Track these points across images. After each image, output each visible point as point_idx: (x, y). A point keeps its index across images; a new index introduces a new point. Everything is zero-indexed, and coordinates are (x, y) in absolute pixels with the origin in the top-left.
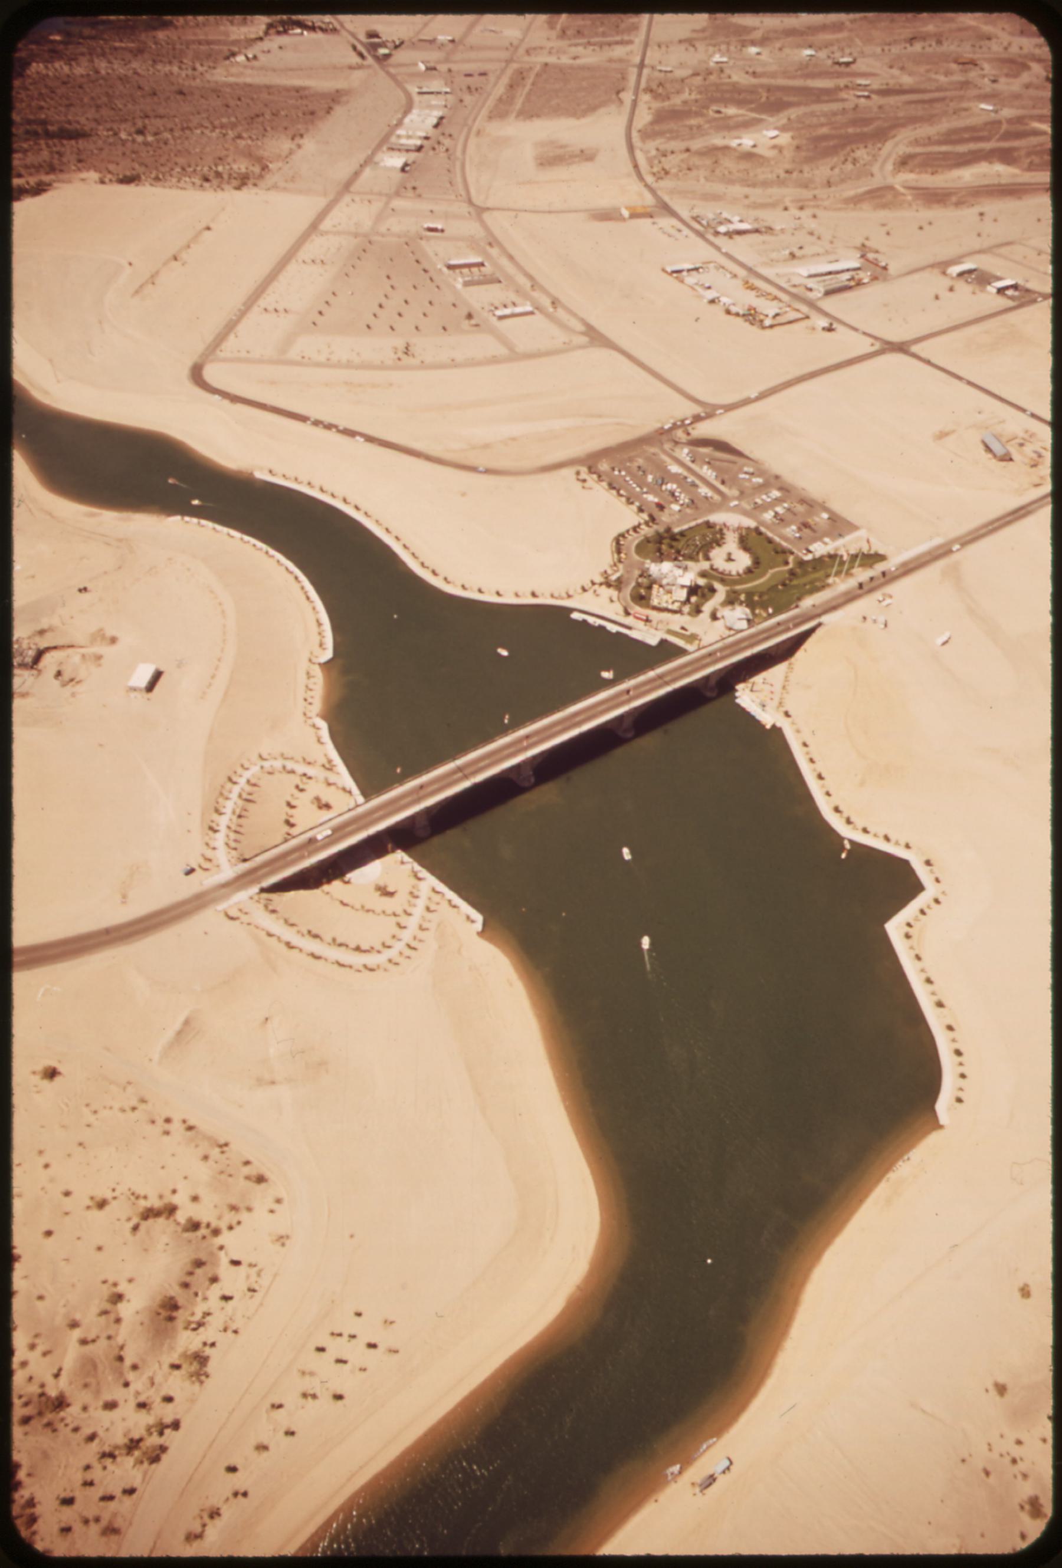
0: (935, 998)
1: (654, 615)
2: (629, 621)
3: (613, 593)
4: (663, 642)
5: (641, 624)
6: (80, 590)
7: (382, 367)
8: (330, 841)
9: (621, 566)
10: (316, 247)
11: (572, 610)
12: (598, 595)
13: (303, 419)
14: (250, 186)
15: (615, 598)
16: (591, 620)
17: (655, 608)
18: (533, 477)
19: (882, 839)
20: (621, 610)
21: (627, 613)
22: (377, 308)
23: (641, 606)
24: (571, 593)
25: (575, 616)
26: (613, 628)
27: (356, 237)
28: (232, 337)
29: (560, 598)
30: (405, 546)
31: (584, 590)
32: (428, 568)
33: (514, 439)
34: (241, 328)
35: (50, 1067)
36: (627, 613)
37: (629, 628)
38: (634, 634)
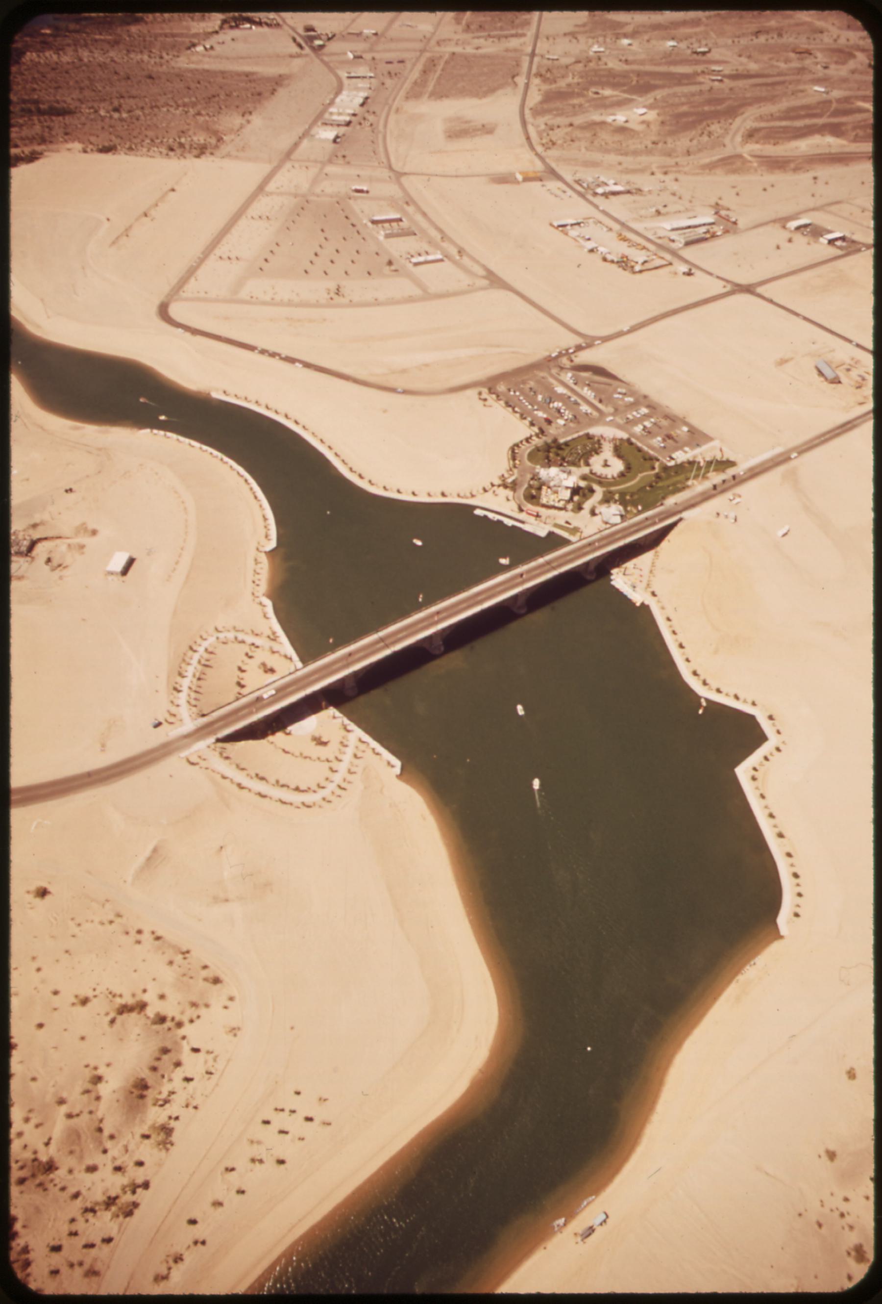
0: (777, 830)
1: (543, 511)
2: (522, 516)
3: (509, 493)
4: (551, 534)
5: (532, 519)
6: (67, 491)
7: (317, 305)
8: (274, 699)
9: (515, 471)
10: (262, 205)
11: (475, 507)
12: (496, 495)
13: (252, 348)
14: (208, 155)
15: (511, 498)
16: (491, 515)
17: (544, 506)
18: (442, 397)
20: (516, 508)
21: (521, 510)
22: (313, 256)
23: (532, 504)
24: (474, 493)
25: (478, 512)
26: (509, 522)
27: (295, 197)
28: (192, 280)
29: (465, 497)
30: (336, 454)
31: (485, 490)
32: (355, 472)
33: (427, 365)
35: (41, 887)
36: (521, 510)
37: (523, 522)
38: (526, 527)
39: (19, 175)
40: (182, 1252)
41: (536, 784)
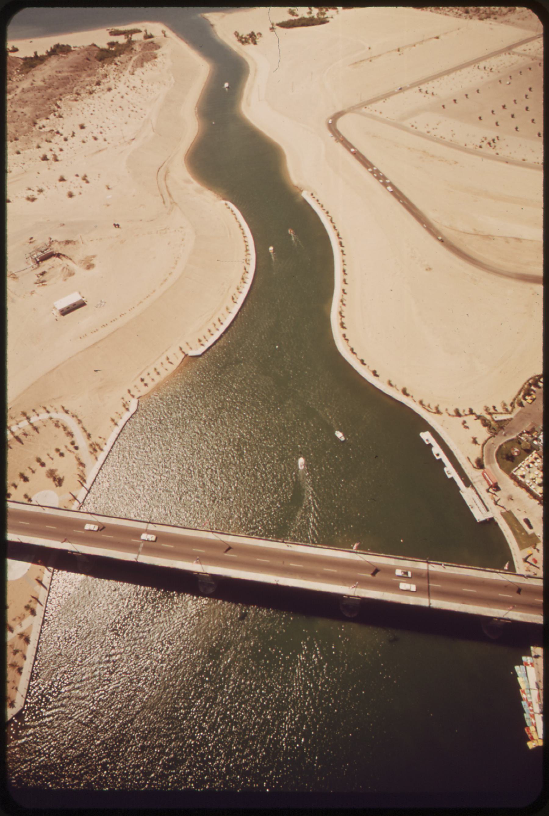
0: (325, 211)
1: (507, 484)
2: (473, 474)
3: (483, 433)
4: (491, 522)
5: (482, 487)
7: (464, 149)
9: (518, 409)
10: (493, 62)
12: (467, 427)
14: (492, 19)
15: (480, 441)
16: (437, 450)
17: (514, 478)
19: (418, 403)
20: (476, 452)
21: (480, 465)
23: (501, 467)
24: (441, 409)
25: (426, 436)
26: (450, 471)
27: (533, 60)
28: (381, 101)
29: (427, 408)
30: (341, 244)
31: (458, 414)
32: (336, 230)
33: (518, 240)
34: (390, 100)
36: (480, 465)
37: (468, 483)
38: (467, 494)
40: (58, 311)
41: (271, 248)
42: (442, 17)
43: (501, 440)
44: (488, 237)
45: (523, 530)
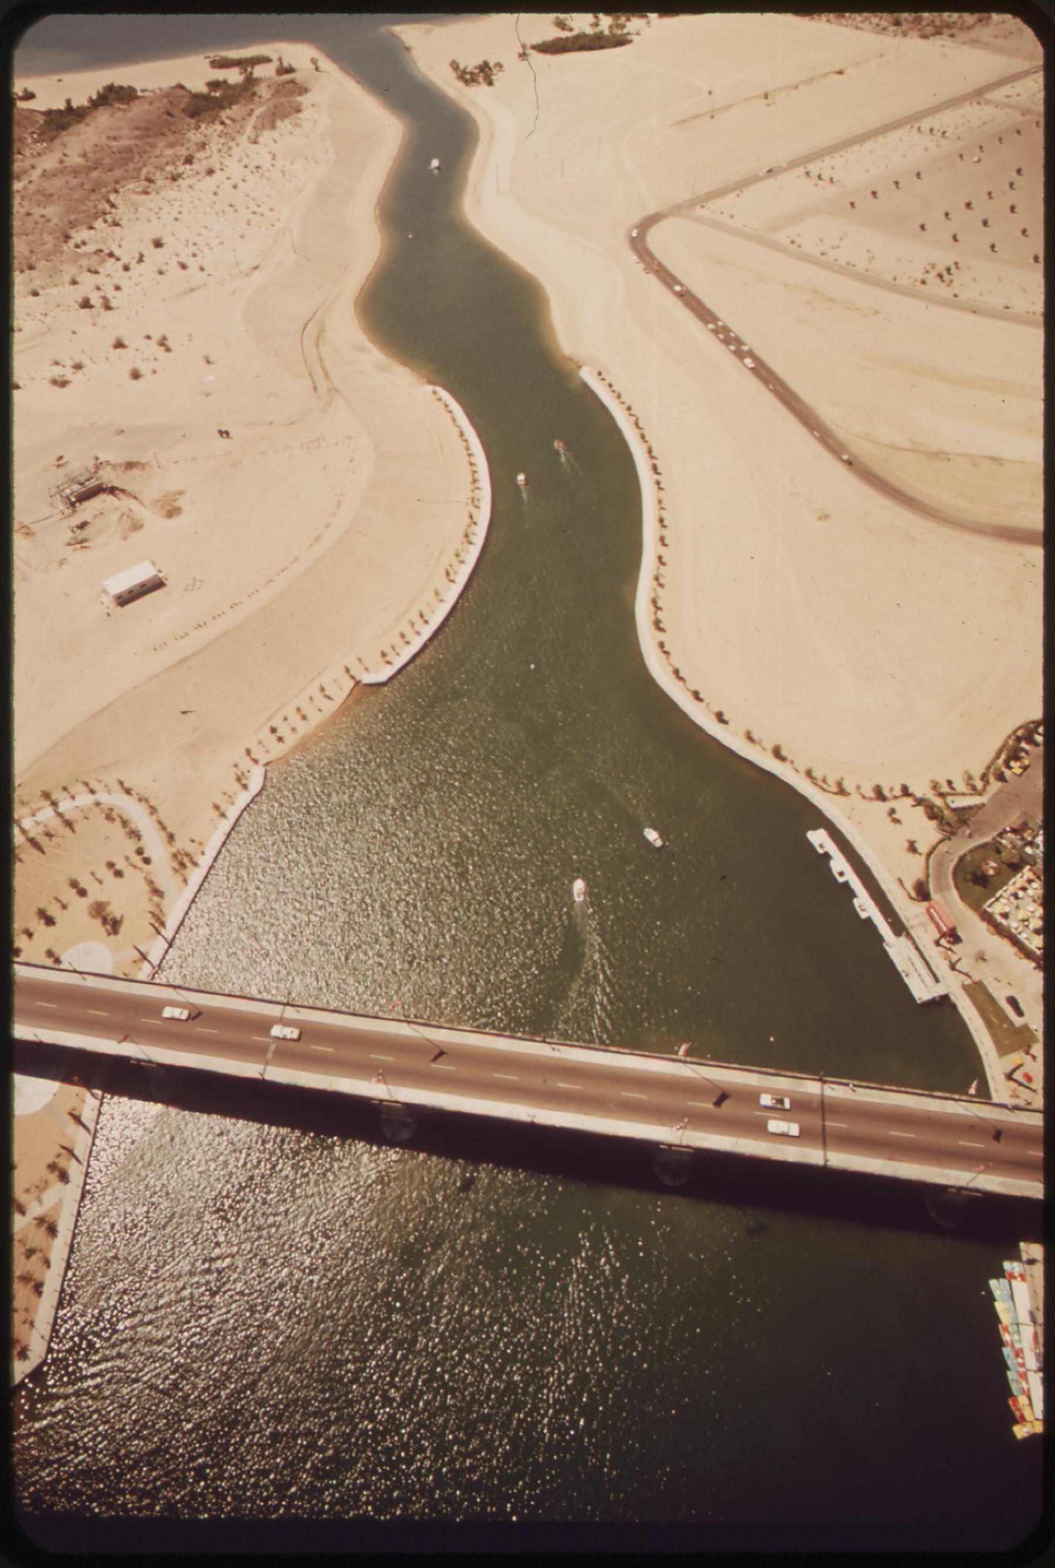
0: (625, 406)
1: (975, 930)
2: (910, 911)
3: (928, 833)
4: (944, 1002)
5: (926, 936)
6: (221, 432)
7: (893, 287)
8: (287, 1053)
9: (995, 786)
11: (821, 821)
12: (897, 821)
13: (687, 298)
14: (945, 37)
15: (923, 847)
16: (839, 864)
17: (987, 918)
18: (973, 539)
19: (803, 774)
20: (914, 868)
21: (922, 893)
22: (1015, 174)
23: (963, 897)
24: (848, 786)
25: (818, 838)
26: (865, 905)
29: (820, 784)
30: (655, 468)
32: (646, 442)
33: (996, 460)
35: (92, 906)
36: (922, 893)
37: (899, 928)
38: (897, 949)
39: (1036, 712)
42: (850, 32)
43: (963, 846)
44: (938, 455)
45: (1005, 1018)
